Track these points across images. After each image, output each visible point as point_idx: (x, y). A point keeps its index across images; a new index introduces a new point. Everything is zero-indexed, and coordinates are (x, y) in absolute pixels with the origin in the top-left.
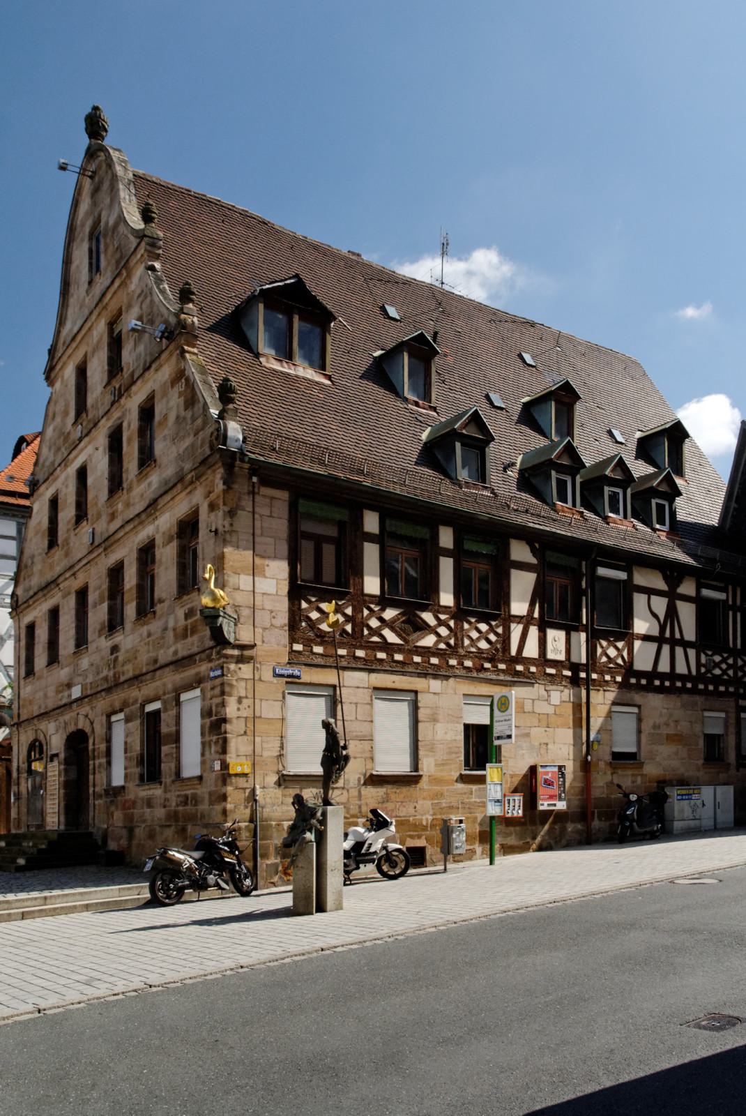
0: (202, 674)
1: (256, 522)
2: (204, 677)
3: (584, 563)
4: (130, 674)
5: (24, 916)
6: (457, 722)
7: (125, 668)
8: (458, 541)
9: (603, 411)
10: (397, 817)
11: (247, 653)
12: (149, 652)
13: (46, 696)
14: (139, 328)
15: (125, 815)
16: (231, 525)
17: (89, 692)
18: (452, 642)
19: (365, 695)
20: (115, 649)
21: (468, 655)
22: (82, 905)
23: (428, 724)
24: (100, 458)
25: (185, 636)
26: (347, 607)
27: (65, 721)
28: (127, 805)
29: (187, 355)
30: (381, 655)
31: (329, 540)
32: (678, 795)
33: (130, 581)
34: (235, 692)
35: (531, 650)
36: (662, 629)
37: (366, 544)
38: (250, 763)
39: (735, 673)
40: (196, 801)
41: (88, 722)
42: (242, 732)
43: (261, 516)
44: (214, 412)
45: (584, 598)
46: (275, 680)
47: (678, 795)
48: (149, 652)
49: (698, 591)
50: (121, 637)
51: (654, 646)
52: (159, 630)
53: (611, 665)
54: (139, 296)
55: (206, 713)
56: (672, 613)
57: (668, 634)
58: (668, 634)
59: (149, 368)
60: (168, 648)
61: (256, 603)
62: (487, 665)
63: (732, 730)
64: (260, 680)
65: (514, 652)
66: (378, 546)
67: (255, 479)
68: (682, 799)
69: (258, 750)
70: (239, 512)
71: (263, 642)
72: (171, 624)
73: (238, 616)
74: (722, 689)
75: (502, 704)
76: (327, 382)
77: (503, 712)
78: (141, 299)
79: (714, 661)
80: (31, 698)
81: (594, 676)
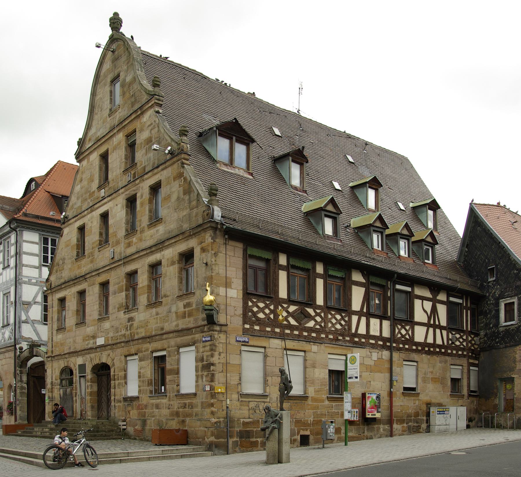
0: (196, 339)
1: (227, 259)
2: (198, 340)
3: (389, 282)
4: (143, 335)
5: (149, 459)
6: (325, 369)
7: (139, 331)
8: (325, 270)
9: (391, 190)
10: (296, 419)
11: (224, 328)
12: (157, 323)
13: (74, 342)
14: (158, 149)
15: (139, 414)
16: (216, 261)
17: (110, 342)
18: (323, 325)
19: (279, 353)
20: (131, 319)
21: (331, 332)
22: (147, 457)
23: (311, 369)
24: (119, 210)
25: (184, 317)
26: (271, 305)
27: (90, 357)
28: (141, 407)
29: (185, 166)
30: (288, 331)
31: (260, 269)
32: (438, 411)
33: (142, 282)
34: (217, 349)
35: (362, 330)
36: (429, 318)
37: (280, 271)
38: (224, 387)
39: (467, 344)
40: (192, 406)
41: (109, 359)
42: (221, 371)
43: (230, 256)
44: (206, 200)
45: (389, 302)
46: (236, 344)
47: (438, 411)
48: (157, 323)
49: (448, 298)
50: (136, 313)
51: (426, 328)
52: (165, 312)
53: (403, 339)
54: (149, 126)
55: (199, 360)
56: (434, 310)
57: (432, 322)
58: (432, 322)
59: (158, 167)
60: (171, 322)
61: (227, 302)
62: (340, 338)
63: (465, 376)
64: (229, 343)
65: (353, 331)
66: (286, 272)
67: (226, 236)
68: (440, 414)
69: (228, 381)
70: (219, 254)
71: (231, 323)
72: (174, 309)
73: (219, 309)
74: (460, 353)
75: (354, 360)
76: (251, 177)
77: (353, 364)
78: (150, 128)
79: (456, 338)
80: (62, 342)
81: (394, 345)
